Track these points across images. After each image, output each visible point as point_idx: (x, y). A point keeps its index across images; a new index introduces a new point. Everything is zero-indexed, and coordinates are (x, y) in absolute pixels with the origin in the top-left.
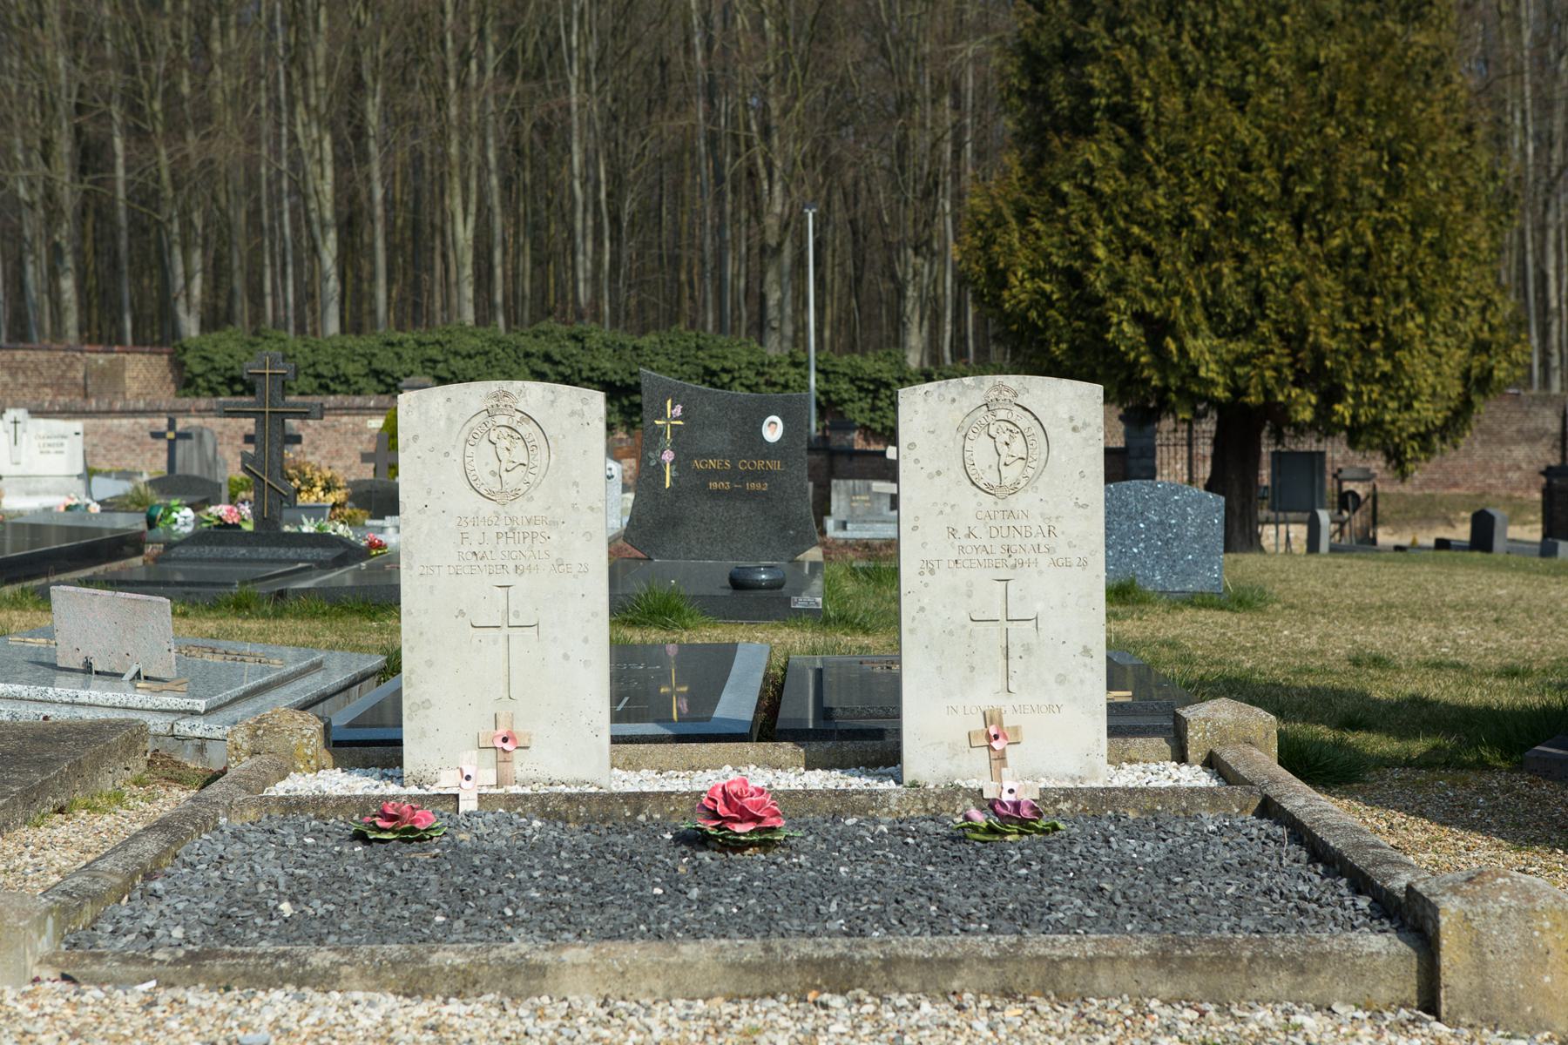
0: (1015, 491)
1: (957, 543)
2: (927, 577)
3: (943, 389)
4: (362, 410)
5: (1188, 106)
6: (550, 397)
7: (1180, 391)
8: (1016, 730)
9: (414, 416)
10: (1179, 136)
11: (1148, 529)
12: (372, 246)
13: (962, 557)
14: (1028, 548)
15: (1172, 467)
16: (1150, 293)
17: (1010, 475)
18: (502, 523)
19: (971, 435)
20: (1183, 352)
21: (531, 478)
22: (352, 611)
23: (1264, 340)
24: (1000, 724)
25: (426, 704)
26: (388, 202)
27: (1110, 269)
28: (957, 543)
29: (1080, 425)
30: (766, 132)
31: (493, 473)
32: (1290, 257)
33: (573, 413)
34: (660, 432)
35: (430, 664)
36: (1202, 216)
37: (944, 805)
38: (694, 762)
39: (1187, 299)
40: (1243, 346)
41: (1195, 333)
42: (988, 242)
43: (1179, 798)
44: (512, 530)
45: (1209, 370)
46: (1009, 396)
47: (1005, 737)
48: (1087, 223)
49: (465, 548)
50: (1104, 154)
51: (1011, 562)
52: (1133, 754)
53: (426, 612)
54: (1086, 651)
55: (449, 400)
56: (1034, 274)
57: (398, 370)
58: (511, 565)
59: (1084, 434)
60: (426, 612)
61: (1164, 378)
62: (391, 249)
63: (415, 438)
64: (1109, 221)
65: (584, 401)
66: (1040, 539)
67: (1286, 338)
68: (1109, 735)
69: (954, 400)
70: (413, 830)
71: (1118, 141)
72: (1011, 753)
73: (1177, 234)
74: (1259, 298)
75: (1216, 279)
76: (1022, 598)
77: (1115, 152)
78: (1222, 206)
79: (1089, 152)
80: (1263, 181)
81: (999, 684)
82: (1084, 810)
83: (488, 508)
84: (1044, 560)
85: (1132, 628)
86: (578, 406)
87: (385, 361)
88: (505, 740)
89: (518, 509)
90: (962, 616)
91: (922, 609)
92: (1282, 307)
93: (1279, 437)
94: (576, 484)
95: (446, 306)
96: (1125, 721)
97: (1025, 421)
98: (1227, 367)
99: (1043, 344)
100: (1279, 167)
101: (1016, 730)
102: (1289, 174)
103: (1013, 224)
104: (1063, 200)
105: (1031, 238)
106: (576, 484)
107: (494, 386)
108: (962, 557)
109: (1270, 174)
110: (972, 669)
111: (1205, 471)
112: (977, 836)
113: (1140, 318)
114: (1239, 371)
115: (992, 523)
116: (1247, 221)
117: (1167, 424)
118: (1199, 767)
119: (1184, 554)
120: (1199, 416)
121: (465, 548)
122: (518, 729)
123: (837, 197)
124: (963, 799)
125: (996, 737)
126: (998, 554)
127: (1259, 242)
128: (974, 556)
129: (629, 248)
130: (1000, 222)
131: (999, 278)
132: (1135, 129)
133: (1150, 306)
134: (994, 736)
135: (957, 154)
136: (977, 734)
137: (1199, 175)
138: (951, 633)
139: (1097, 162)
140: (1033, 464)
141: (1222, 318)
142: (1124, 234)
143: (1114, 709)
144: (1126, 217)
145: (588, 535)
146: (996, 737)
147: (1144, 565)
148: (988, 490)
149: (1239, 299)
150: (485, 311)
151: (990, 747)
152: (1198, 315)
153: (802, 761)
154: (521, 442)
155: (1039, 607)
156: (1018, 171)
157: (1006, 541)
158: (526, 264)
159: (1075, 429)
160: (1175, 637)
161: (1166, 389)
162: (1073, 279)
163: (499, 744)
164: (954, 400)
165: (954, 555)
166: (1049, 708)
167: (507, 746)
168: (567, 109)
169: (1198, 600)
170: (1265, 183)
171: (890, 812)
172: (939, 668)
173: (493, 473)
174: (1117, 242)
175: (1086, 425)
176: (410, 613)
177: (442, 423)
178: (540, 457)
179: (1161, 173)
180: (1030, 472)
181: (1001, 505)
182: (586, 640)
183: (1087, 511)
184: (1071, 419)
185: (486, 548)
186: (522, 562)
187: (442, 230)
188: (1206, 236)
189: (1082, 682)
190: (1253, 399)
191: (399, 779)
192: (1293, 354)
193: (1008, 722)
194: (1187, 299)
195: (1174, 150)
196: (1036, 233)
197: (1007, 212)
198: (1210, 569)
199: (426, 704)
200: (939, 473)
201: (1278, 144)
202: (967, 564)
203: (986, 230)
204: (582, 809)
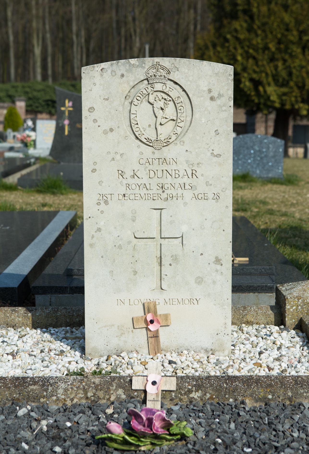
0: (167, 144)
1: (125, 182)
2: (103, 206)
3: (115, 67)
5: (269, 10)
7: (265, 104)
8: (166, 317)
10: (265, 20)
11: (254, 153)
13: (128, 192)
14: (177, 186)
15: (260, 129)
16: (255, 72)
17: (165, 131)
19: (136, 102)
20: (265, 91)
23: (291, 88)
24: (155, 313)
27: (242, 64)
28: (125, 182)
29: (216, 95)
30: (134, 19)
32: (301, 60)
34: (63, 112)
36: (272, 46)
37: (101, 394)
39: (267, 74)
40: (285, 90)
41: (269, 84)
43: (286, 389)
45: (274, 98)
46: (163, 73)
47: (158, 322)
48: (235, 48)
50: (241, 26)
51: (164, 196)
52: (250, 318)
54: (218, 261)
59: (219, 102)
61: (259, 100)
64: (242, 48)
66: (185, 180)
67: (299, 87)
68: (233, 291)
69: (123, 76)
71: (246, 21)
72: (163, 334)
73: (264, 52)
74: (290, 74)
75: (276, 67)
76: (172, 222)
77: (245, 25)
78: (279, 42)
79: (236, 25)
80: (293, 35)
81: (155, 283)
82: (211, 398)
84: (188, 194)
85: (248, 193)
90: (128, 234)
91: (99, 230)
92: (297, 77)
93: (295, 119)
96: (246, 281)
97: (175, 92)
98: (280, 97)
100: (298, 30)
101: (166, 317)
102: (301, 33)
103: (211, 48)
104: (227, 40)
105: (217, 54)
108: (128, 192)
109: (295, 33)
110: (135, 273)
111: (271, 131)
112: (116, 446)
113: (252, 80)
114: (284, 98)
115: (151, 167)
116: (287, 48)
117: (259, 115)
118: (293, 332)
119: (268, 163)
120: (270, 113)
123: (158, 43)
124: (116, 390)
125: (152, 322)
126: (155, 190)
127: (291, 56)
128: (137, 191)
132: (252, 17)
133: (255, 76)
134: (150, 320)
135: (195, 28)
136: (138, 319)
137: (272, 33)
138: (120, 247)
139: (239, 28)
140: (181, 124)
141: (278, 81)
142: (247, 52)
143: (237, 271)
144: (248, 47)
146: (152, 322)
147: (252, 167)
148: (148, 143)
149: (284, 74)
150: (45, 77)
151: (147, 329)
152: (270, 79)
153: (30, 322)
154: (171, 103)
155: (184, 228)
156: (213, 31)
157: (161, 181)
159: (212, 99)
160: (265, 198)
161: (259, 104)
164: (123, 76)
165: (123, 190)
166: (191, 301)
168: (71, 12)
169: (273, 181)
170: (293, 36)
171: (58, 399)
172: (111, 272)
174: (244, 55)
175: (220, 96)
179: (259, 32)
180: (179, 130)
181: (157, 154)
183: (220, 160)
184: (210, 91)
188: (273, 53)
189: (214, 282)
190: (288, 107)
192: (301, 92)
193: (160, 311)
194: (267, 74)
195: (264, 24)
196: (219, 52)
197: (210, 45)
198: (278, 169)
200: (111, 130)
201: (298, 23)
202: (132, 197)
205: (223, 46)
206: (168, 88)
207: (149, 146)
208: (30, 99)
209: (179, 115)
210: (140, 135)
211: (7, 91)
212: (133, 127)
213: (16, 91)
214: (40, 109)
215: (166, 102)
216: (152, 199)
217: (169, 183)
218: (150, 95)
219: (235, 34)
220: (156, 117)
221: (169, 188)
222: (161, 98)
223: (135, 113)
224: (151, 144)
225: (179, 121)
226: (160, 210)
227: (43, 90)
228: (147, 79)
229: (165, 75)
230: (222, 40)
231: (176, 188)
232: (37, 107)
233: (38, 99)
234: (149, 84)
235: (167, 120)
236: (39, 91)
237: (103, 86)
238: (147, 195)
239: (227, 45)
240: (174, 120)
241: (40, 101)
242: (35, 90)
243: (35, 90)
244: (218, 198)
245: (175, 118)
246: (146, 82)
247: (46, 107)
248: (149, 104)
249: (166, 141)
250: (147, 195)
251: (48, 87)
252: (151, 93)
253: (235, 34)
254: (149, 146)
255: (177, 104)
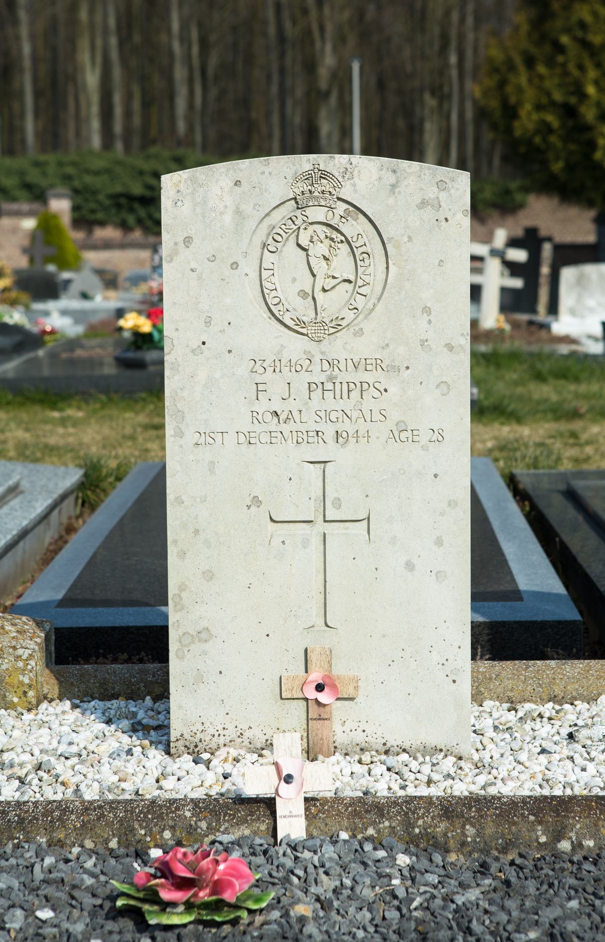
4: (19, 214)
6: (390, 178)
9: (186, 209)
12: (21, 93)
18: (316, 368)
21: (360, 302)
22: (33, 401)
25: (204, 635)
26: (35, 59)
31: (303, 294)
33: (424, 204)
35: (209, 575)
38: (557, 691)
42: (502, 84)
44: (331, 379)
49: (262, 407)
53: (204, 500)
55: (237, 183)
56: (539, 107)
57: (43, 183)
58: (329, 431)
60: (204, 500)
62: (37, 94)
63: (188, 241)
65: (441, 185)
70: (218, 906)
83: (295, 346)
86: (432, 193)
87: (34, 176)
88: (320, 688)
89: (339, 347)
94: (427, 310)
95: (78, 134)
99: (544, 163)
103: (522, 68)
104: (560, 49)
105: (536, 81)
106: (427, 310)
107: (305, 162)
121: (262, 407)
122: (340, 670)
129: (214, 92)
130: (511, 66)
131: (511, 112)
135: (462, 20)
139: (588, 18)
145: (444, 386)
148: (297, 328)
154: (345, 248)
156: (525, 28)
158: (136, 105)
162: (569, 112)
163: (311, 694)
167: (323, 697)
173: (303, 294)
176: (179, 501)
177: (228, 218)
178: (375, 268)
180: (360, 302)
182: (439, 542)
185: (293, 405)
186: (347, 426)
187: (73, 77)
191: (156, 731)
196: (541, 77)
197: (518, 60)
199: (204, 635)
203: (501, 73)
204: (470, 830)
205: (550, 63)
206: (337, 217)
207: (298, 332)
208: (76, 192)
209: (360, 270)
210: (281, 313)
211: (22, 173)
212: (267, 296)
213: (44, 174)
214: (100, 216)
215: (333, 244)
216: (305, 441)
217: (339, 409)
218: (301, 230)
219: (579, 34)
220: (314, 275)
221: (340, 420)
222: (322, 236)
223: (271, 267)
224: (304, 331)
225: (360, 282)
226: (323, 465)
227: (108, 171)
228: (295, 199)
229: (331, 190)
230: (548, 48)
231: (354, 419)
232: (93, 211)
233: (95, 193)
234: (298, 208)
235: (337, 281)
236: (97, 173)
237: (214, 208)
238: (295, 434)
239: (560, 59)
240: (349, 281)
241: (101, 197)
242: (88, 171)
243: (88, 171)
244: (440, 438)
245: (352, 278)
246: (293, 202)
247: (113, 211)
248: (299, 250)
249: (334, 323)
250: (295, 434)
251: (118, 163)
252: (303, 227)
253: (579, 34)
254: (298, 332)
255: (355, 249)
